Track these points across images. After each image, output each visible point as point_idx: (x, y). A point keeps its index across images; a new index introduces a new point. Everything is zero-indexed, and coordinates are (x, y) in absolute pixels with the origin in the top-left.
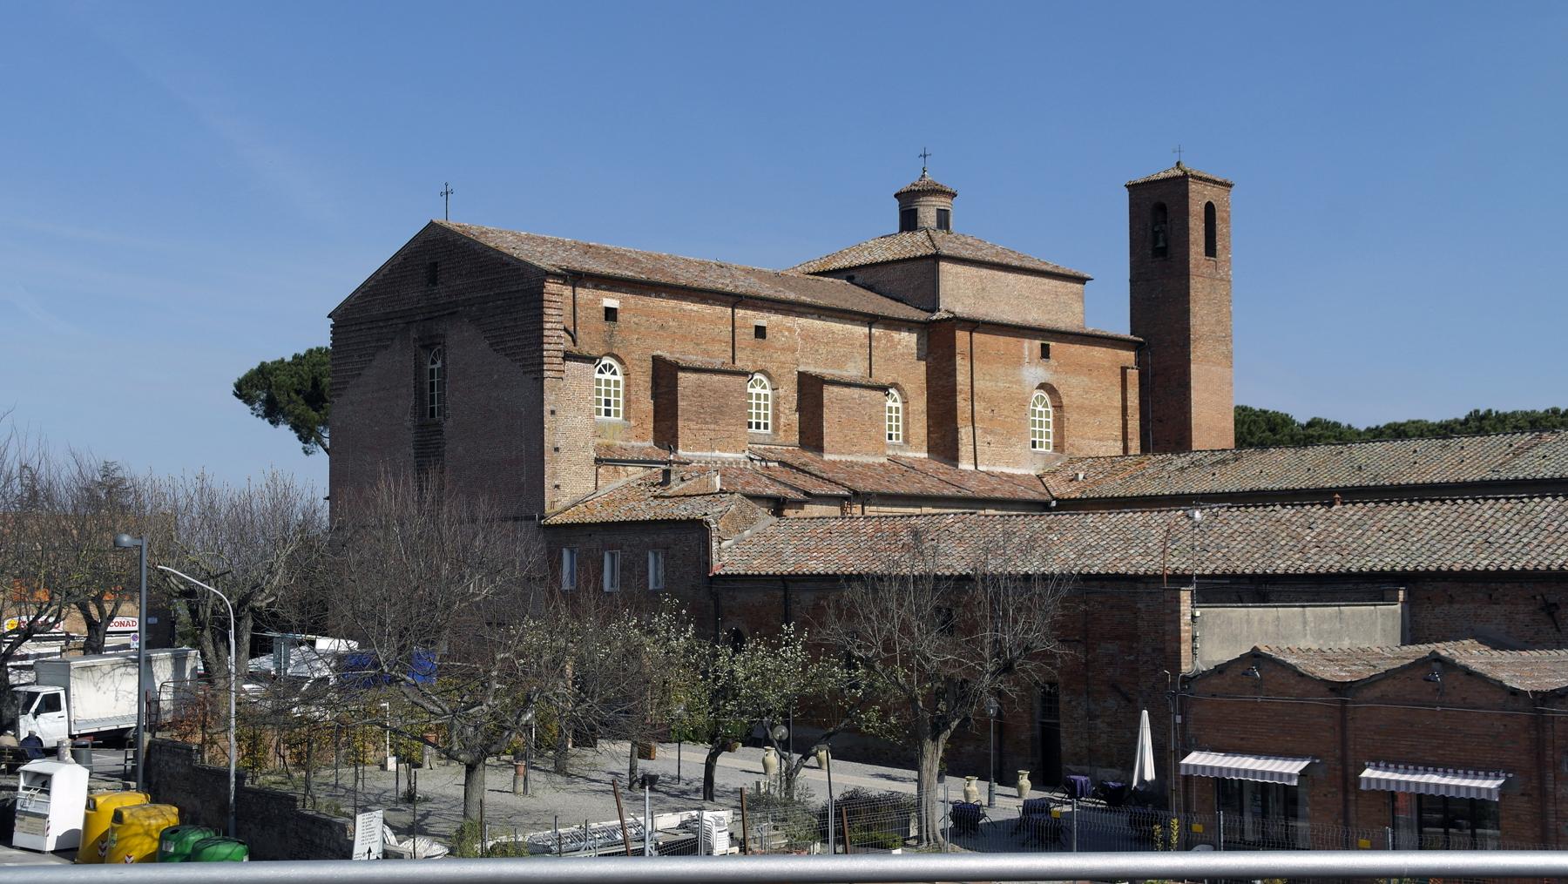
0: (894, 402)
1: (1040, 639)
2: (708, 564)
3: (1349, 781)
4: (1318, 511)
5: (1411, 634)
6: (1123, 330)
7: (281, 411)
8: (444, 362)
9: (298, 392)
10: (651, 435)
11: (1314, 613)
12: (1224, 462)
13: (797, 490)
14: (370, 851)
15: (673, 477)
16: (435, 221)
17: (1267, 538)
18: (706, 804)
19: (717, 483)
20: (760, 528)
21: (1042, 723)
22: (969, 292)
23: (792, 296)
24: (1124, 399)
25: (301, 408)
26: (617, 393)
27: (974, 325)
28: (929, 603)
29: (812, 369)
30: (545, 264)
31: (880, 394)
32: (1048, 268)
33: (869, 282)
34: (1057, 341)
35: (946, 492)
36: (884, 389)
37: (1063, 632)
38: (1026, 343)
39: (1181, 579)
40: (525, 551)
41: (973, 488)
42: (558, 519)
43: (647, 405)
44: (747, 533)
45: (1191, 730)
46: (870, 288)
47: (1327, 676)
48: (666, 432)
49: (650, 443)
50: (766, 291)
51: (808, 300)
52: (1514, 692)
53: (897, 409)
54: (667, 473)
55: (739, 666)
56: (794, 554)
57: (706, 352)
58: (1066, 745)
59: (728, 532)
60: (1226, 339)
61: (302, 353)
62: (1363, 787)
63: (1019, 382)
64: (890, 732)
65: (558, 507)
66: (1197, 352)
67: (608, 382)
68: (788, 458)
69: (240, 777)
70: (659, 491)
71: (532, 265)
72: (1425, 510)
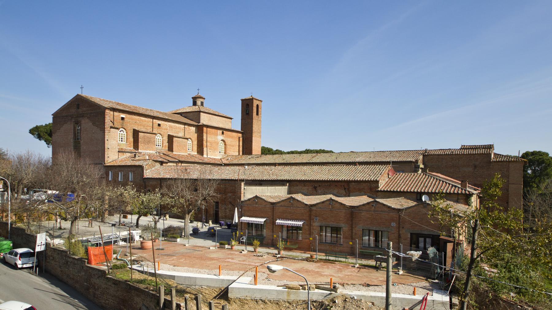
0: (189, 142)
1: (212, 193)
2: (143, 175)
3: (274, 223)
4: (273, 167)
5: (289, 192)
6: (239, 129)
7: (41, 137)
8: (81, 127)
9: (46, 133)
10: (133, 146)
11: (270, 188)
12: (258, 157)
13: (166, 160)
14: (41, 243)
15: (136, 156)
16: (79, 94)
17: (263, 172)
18: (136, 229)
19: (147, 158)
20: (156, 167)
21: (216, 210)
22: (207, 120)
23: (167, 118)
24: (239, 144)
25: (47, 137)
26: (124, 137)
27: (208, 126)
28: (188, 184)
29: (171, 134)
30: (106, 106)
31: (186, 140)
32: (224, 116)
33: (185, 116)
34: (225, 131)
35: (200, 161)
36: (187, 139)
37: (217, 191)
38: (219, 131)
39: (243, 180)
40: (97, 173)
41: (206, 161)
42: (108, 164)
43: (132, 140)
44: (153, 169)
45: (243, 212)
46: (185, 117)
47: (271, 201)
48: (136, 146)
49: (132, 148)
50: (161, 116)
51: (170, 119)
52: (306, 205)
53: (160, 139)
54: (135, 155)
55: (145, 198)
56: (163, 173)
57: (146, 129)
58: (220, 215)
59: (149, 169)
60: (260, 132)
61: (48, 124)
62: (276, 224)
63: (217, 139)
64: (179, 212)
65: (109, 162)
66: (254, 135)
67: (122, 134)
68: (165, 153)
69: (11, 224)
70: (133, 159)
71: (103, 106)
72: (294, 167)
